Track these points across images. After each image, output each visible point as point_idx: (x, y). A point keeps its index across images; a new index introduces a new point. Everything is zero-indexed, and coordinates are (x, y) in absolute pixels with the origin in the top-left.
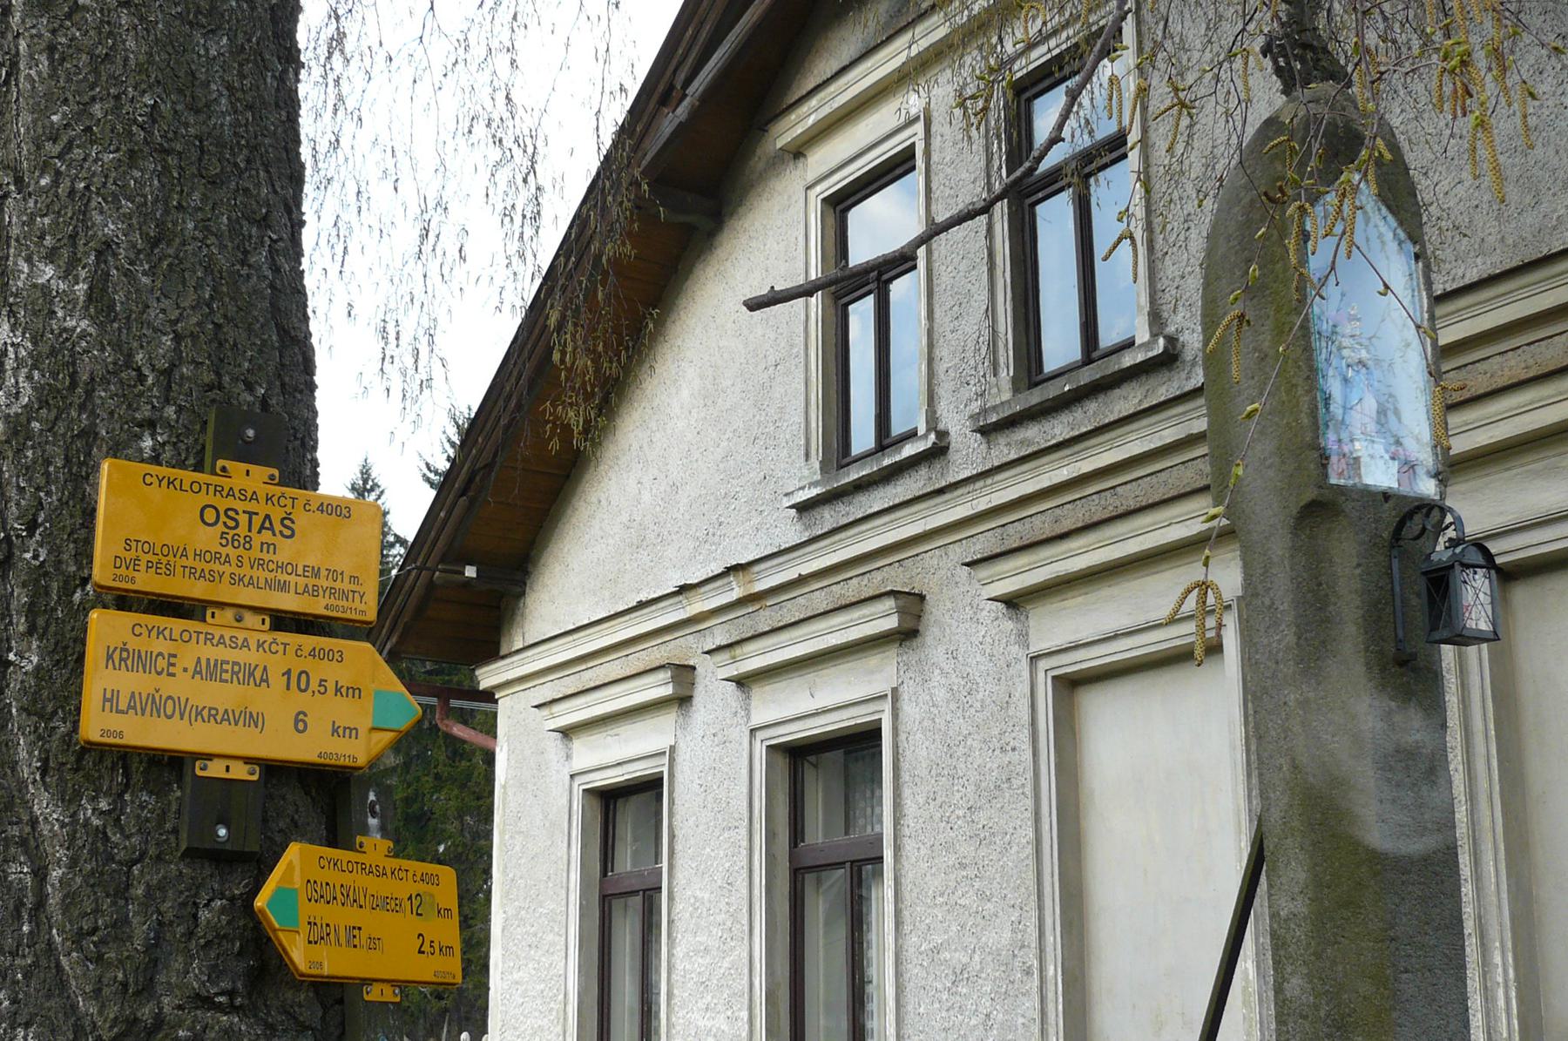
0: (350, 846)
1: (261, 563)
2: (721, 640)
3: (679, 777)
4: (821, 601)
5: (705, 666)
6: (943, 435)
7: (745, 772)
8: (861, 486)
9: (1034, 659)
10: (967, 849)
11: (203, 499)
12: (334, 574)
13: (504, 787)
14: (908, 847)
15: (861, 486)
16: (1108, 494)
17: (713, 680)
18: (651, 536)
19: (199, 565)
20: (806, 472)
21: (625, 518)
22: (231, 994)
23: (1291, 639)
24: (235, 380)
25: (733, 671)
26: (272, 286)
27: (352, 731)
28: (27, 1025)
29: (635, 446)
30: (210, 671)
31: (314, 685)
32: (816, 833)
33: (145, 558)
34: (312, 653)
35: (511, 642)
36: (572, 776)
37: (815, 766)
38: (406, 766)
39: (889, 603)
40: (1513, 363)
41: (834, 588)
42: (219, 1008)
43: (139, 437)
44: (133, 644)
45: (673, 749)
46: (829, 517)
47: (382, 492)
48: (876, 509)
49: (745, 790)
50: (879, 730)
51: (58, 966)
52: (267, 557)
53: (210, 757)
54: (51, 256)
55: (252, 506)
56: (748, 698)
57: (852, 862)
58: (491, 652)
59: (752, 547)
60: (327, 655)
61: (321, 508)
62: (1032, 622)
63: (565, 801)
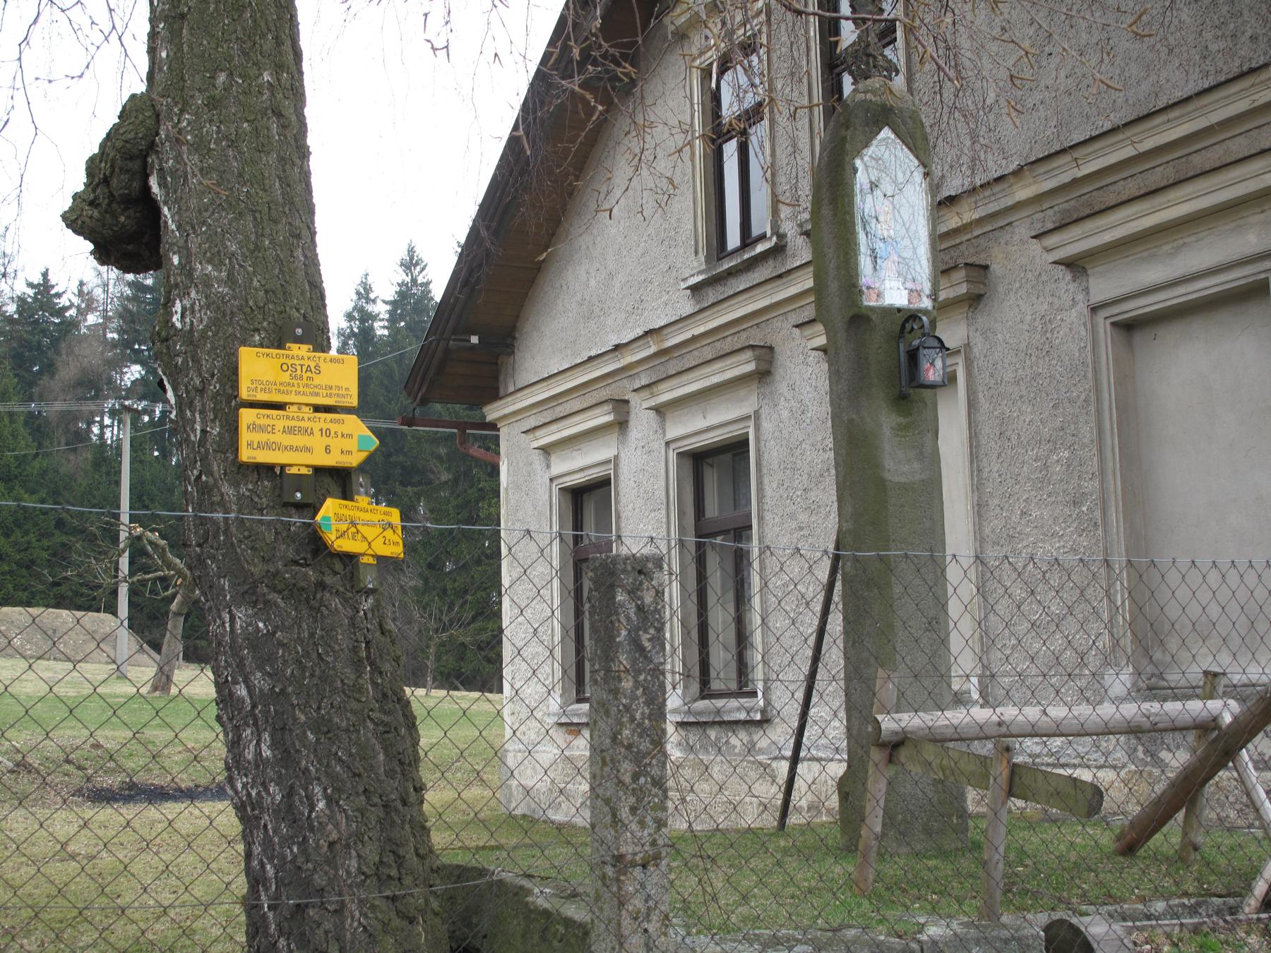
0: (352, 499)
1: (307, 386)
2: (644, 381)
3: (622, 478)
4: (708, 353)
5: (635, 399)
6: (781, 237)
7: (663, 471)
8: (731, 273)
10: (803, 517)
11: (282, 360)
12: (338, 388)
13: (506, 489)
14: (767, 518)
15: (731, 273)
17: (640, 410)
18: (597, 310)
19: (282, 388)
20: (695, 264)
21: (579, 297)
22: (305, 559)
23: (846, 388)
24: (291, 308)
25: (652, 403)
26: (304, 264)
27: (350, 452)
28: (225, 577)
29: (584, 247)
30: (289, 431)
31: (332, 434)
32: (712, 509)
33: (259, 387)
34: (331, 421)
35: (506, 387)
36: (551, 480)
37: (712, 466)
38: (456, 481)
39: (748, 354)
40: (1131, 185)
41: (716, 344)
42: (301, 565)
43: (253, 336)
44: (258, 422)
45: (616, 457)
46: (712, 295)
47: (426, 266)
48: (741, 288)
49: (663, 483)
50: (748, 440)
51: (236, 553)
52: (309, 383)
53: (291, 465)
54: (209, 261)
55: (302, 362)
56: (664, 420)
57: (735, 529)
58: (494, 395)
59: (663, 316)
60: (338, 421)
61: (331, 360)
63: (547, 496)
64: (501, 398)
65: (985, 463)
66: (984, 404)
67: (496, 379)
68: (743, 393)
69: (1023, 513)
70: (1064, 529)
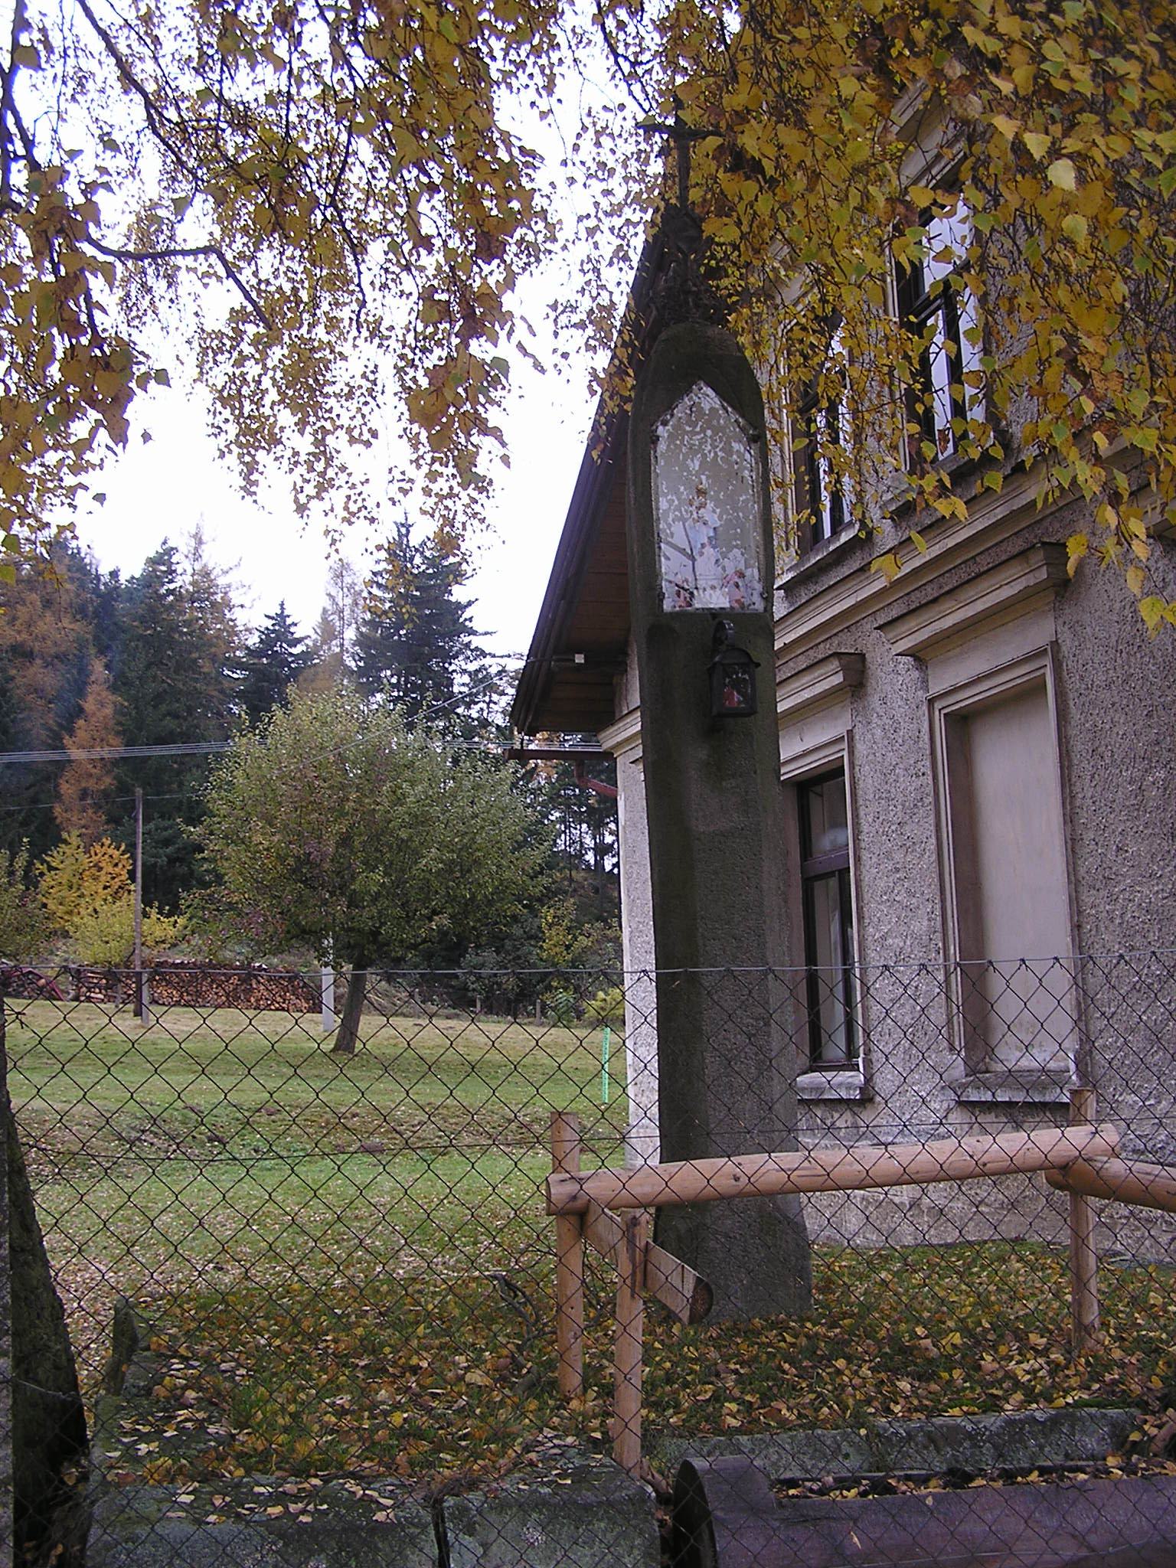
8: (822, 568)
9: (931, 702)
10: (898, 856)
16: (970, 563)
39: (835, 664)
45: (1055, 644)
57: (840, 871)
62: (929, 672)
64: (622, 718)
65: (1077, 789)
66: (1075, 714)
67: (612, 701)
68: (837, 709)
69: (1119, 849)
70: (1163, 868)
